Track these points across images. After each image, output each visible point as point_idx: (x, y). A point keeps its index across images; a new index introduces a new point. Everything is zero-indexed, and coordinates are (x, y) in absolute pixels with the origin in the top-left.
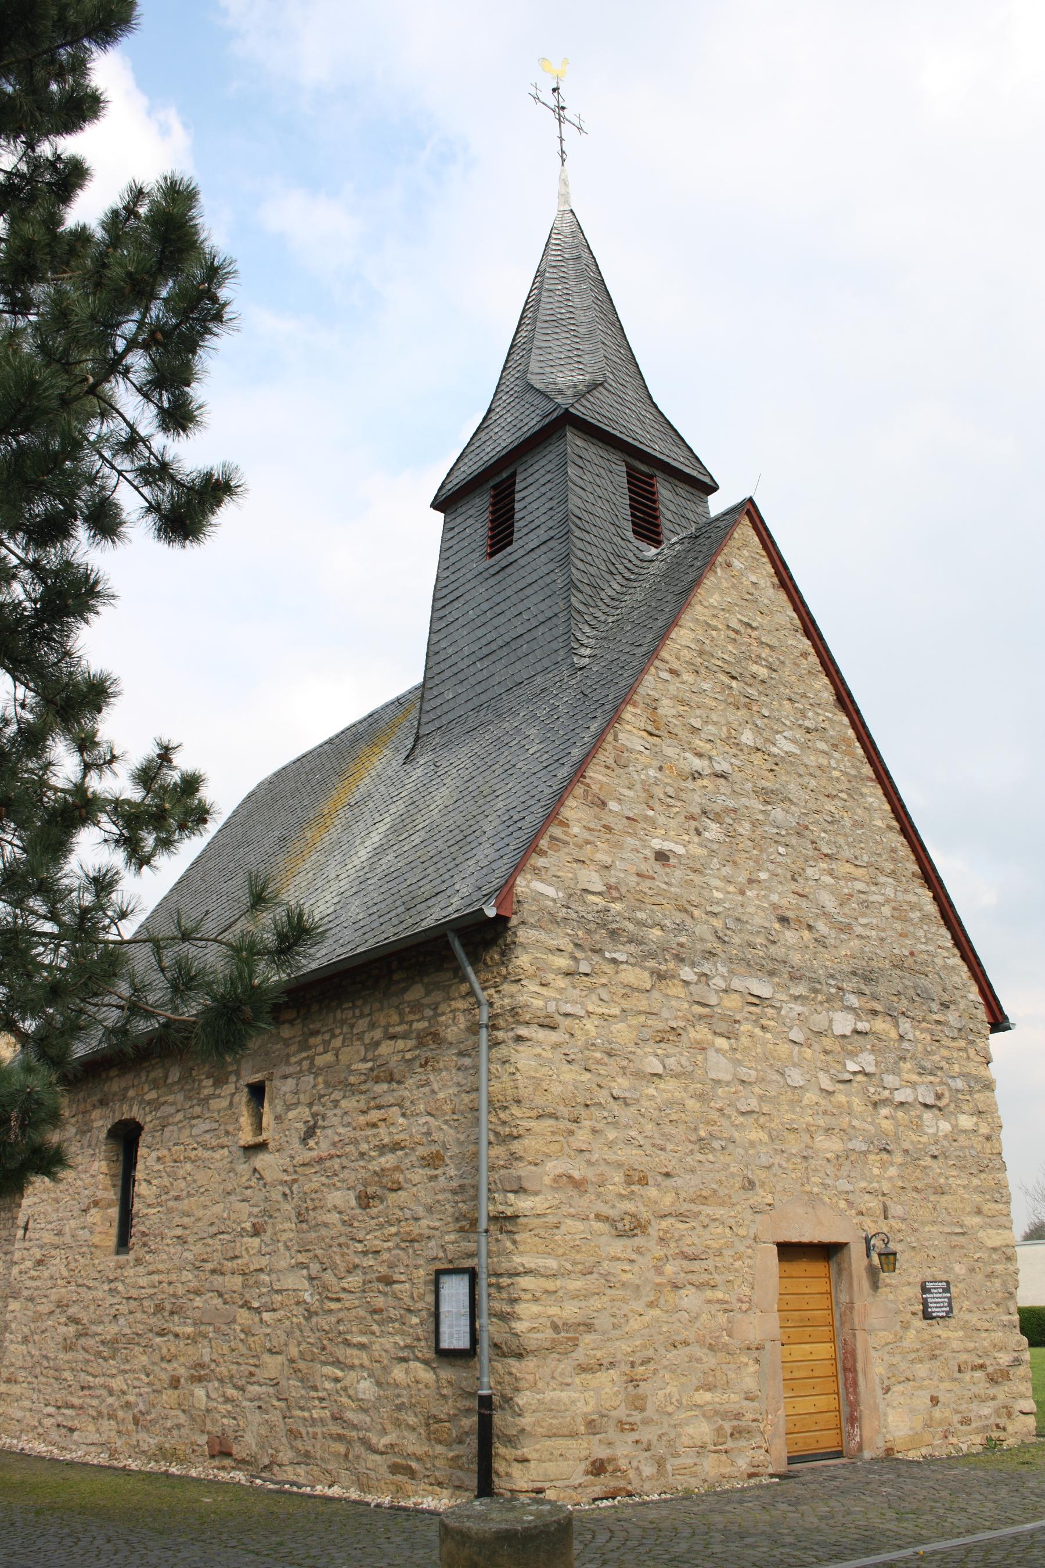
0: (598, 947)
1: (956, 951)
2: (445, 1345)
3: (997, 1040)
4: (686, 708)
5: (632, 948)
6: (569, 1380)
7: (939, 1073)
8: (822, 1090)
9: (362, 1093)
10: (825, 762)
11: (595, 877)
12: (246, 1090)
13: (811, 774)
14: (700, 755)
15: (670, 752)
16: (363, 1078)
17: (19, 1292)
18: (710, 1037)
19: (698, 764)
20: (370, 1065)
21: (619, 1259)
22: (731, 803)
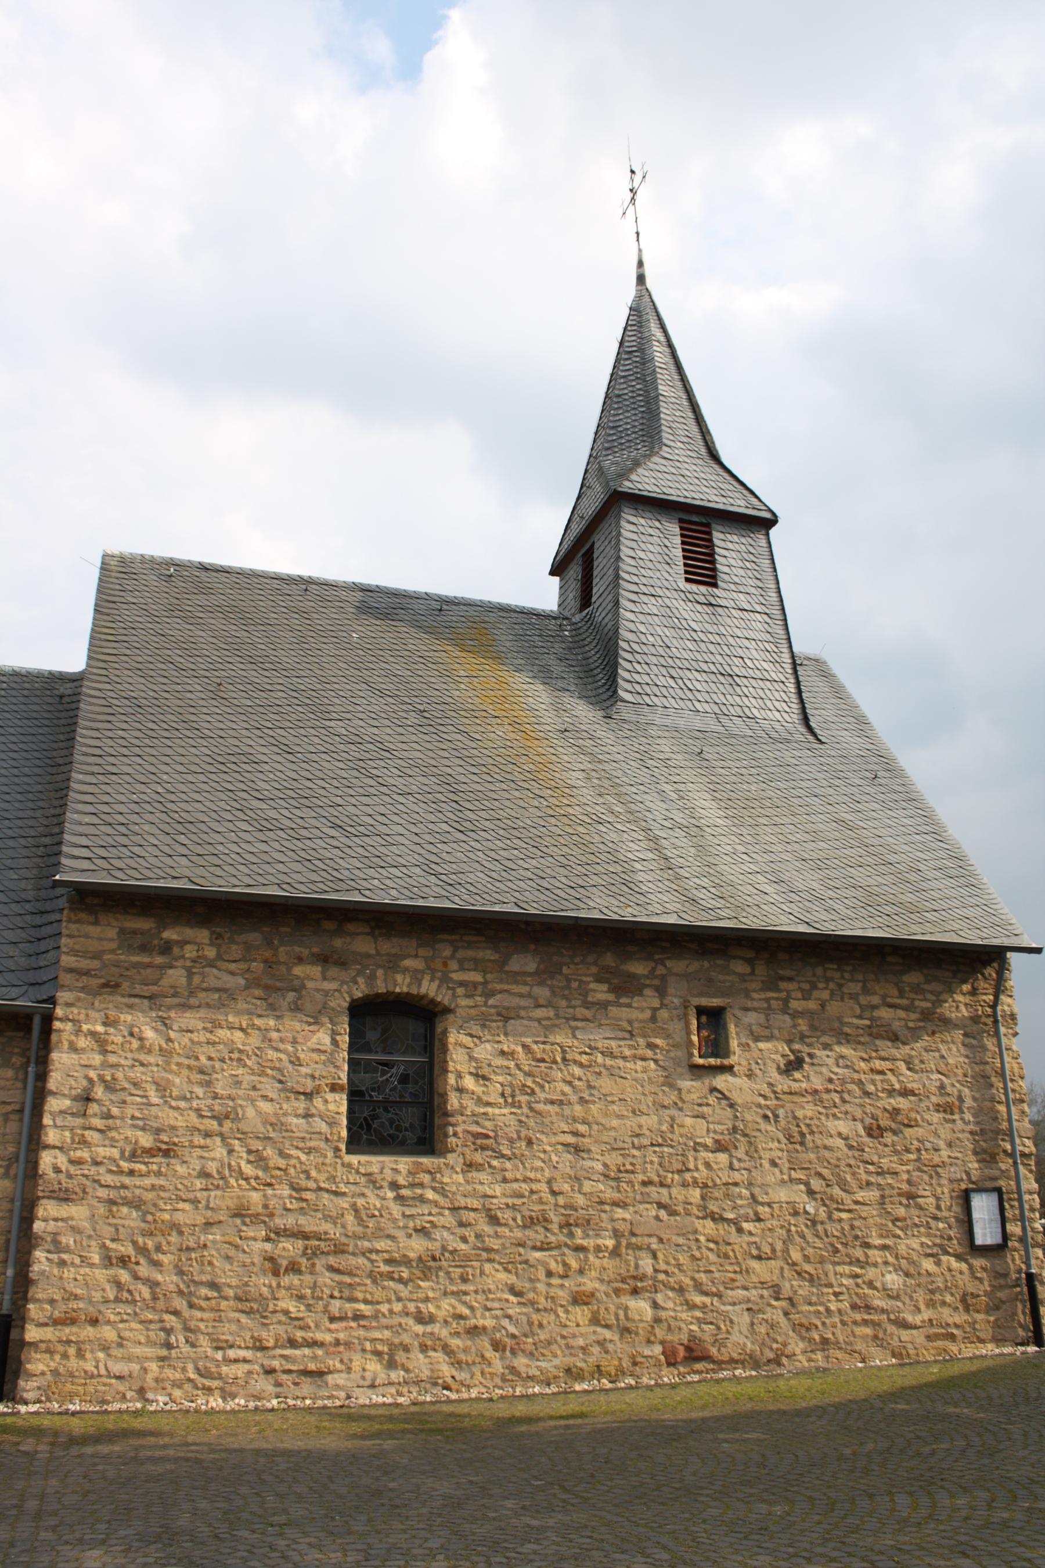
2: (979, 1241)
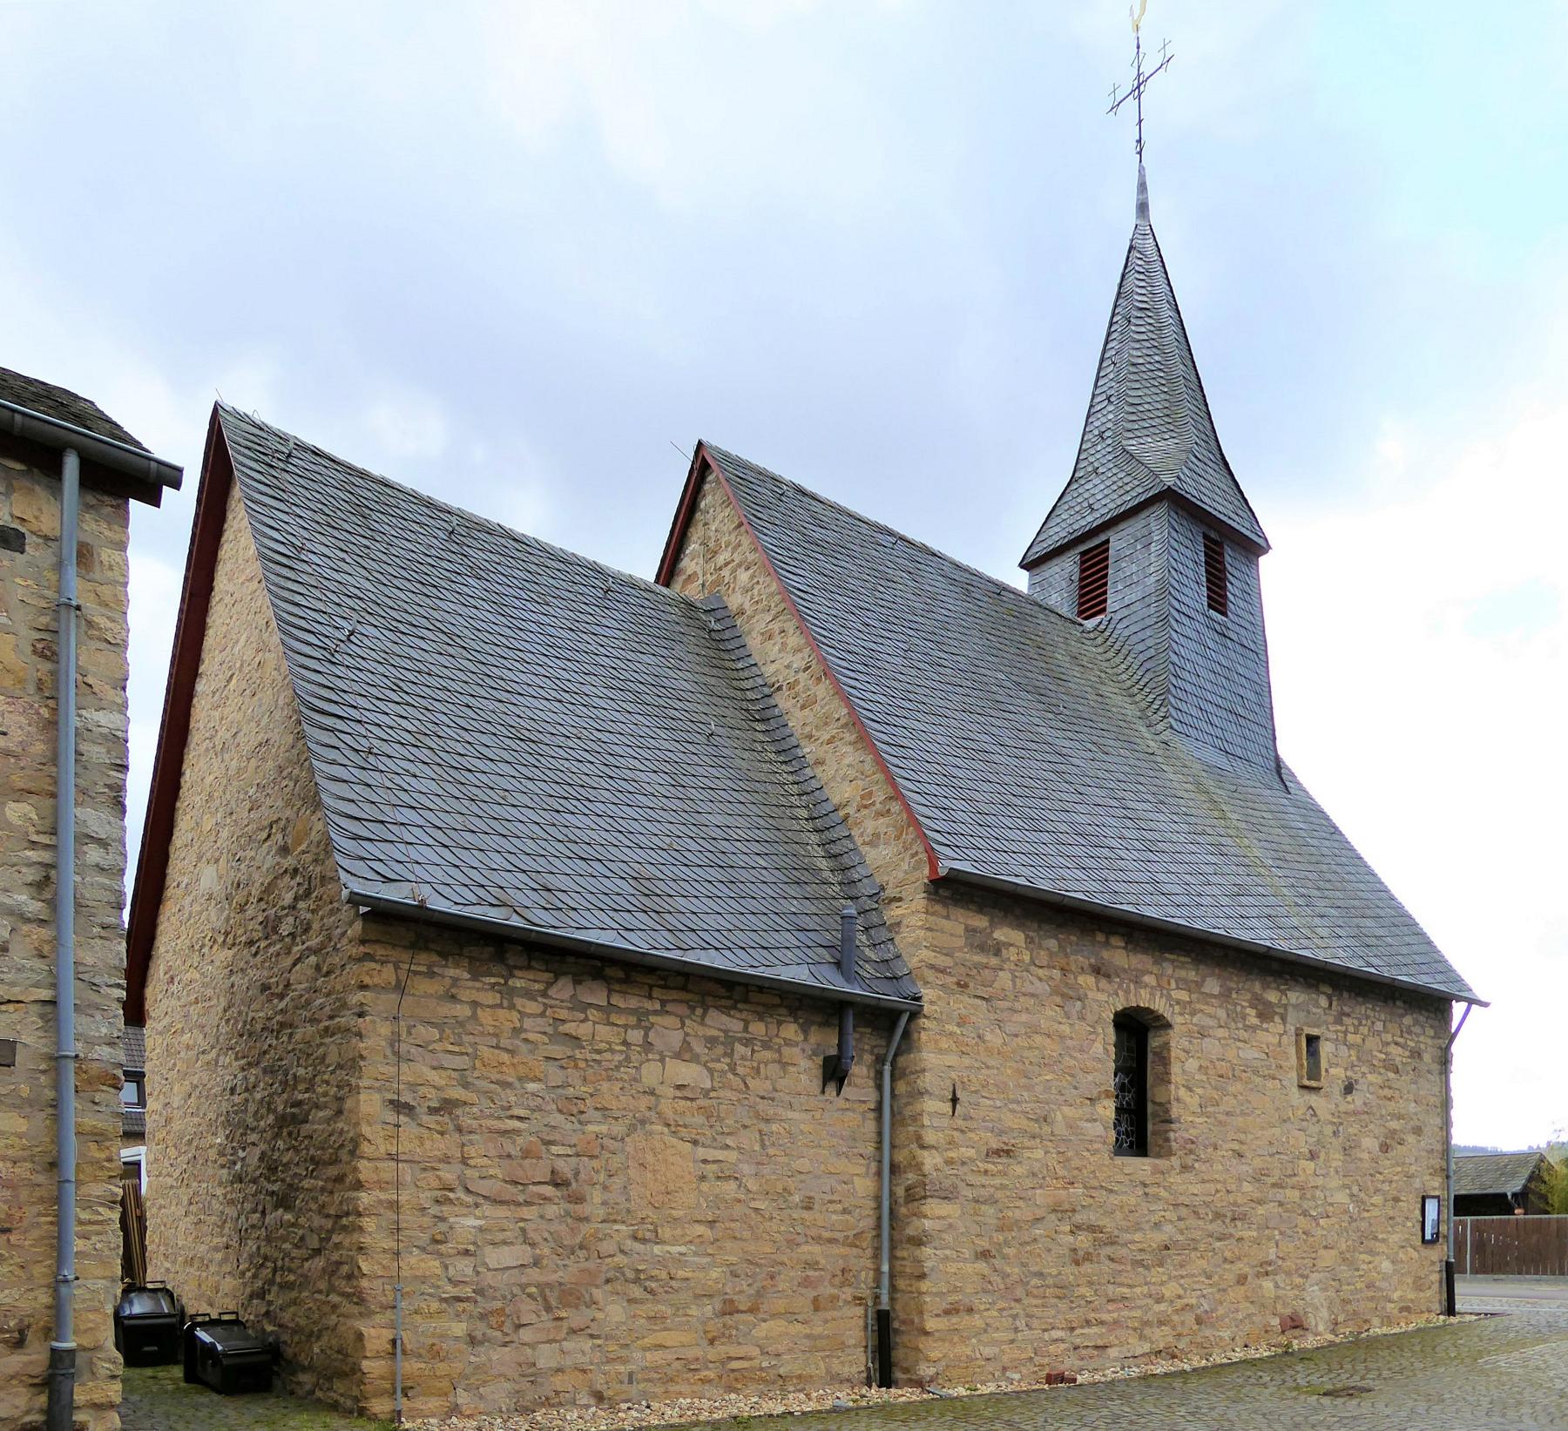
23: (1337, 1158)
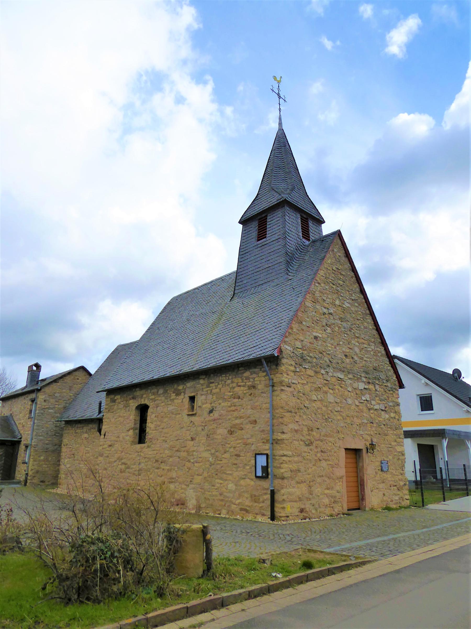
0: (301, 364)
1: (390, 365)
2: (257, 475)
3: (400, 390)
4: (322, 294)
5: (310, 365)
6: (294, 486)
7: (386, 401)
8: (356, 405)
9: (229, 401)
10: (357, 309)
11: (299, 344)
12: (188, 398)
13: (353, 313)
14: (325, 308)
15: (318, 307)
16: (229, 397)
17: (103, 454)
18: (328, 389)
19: (325, 311)
20: (232, 393)
21: (306, 452)
22: (333, 322)
23: (204, 440)
